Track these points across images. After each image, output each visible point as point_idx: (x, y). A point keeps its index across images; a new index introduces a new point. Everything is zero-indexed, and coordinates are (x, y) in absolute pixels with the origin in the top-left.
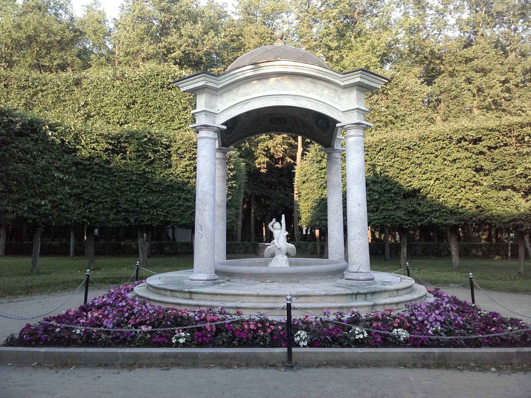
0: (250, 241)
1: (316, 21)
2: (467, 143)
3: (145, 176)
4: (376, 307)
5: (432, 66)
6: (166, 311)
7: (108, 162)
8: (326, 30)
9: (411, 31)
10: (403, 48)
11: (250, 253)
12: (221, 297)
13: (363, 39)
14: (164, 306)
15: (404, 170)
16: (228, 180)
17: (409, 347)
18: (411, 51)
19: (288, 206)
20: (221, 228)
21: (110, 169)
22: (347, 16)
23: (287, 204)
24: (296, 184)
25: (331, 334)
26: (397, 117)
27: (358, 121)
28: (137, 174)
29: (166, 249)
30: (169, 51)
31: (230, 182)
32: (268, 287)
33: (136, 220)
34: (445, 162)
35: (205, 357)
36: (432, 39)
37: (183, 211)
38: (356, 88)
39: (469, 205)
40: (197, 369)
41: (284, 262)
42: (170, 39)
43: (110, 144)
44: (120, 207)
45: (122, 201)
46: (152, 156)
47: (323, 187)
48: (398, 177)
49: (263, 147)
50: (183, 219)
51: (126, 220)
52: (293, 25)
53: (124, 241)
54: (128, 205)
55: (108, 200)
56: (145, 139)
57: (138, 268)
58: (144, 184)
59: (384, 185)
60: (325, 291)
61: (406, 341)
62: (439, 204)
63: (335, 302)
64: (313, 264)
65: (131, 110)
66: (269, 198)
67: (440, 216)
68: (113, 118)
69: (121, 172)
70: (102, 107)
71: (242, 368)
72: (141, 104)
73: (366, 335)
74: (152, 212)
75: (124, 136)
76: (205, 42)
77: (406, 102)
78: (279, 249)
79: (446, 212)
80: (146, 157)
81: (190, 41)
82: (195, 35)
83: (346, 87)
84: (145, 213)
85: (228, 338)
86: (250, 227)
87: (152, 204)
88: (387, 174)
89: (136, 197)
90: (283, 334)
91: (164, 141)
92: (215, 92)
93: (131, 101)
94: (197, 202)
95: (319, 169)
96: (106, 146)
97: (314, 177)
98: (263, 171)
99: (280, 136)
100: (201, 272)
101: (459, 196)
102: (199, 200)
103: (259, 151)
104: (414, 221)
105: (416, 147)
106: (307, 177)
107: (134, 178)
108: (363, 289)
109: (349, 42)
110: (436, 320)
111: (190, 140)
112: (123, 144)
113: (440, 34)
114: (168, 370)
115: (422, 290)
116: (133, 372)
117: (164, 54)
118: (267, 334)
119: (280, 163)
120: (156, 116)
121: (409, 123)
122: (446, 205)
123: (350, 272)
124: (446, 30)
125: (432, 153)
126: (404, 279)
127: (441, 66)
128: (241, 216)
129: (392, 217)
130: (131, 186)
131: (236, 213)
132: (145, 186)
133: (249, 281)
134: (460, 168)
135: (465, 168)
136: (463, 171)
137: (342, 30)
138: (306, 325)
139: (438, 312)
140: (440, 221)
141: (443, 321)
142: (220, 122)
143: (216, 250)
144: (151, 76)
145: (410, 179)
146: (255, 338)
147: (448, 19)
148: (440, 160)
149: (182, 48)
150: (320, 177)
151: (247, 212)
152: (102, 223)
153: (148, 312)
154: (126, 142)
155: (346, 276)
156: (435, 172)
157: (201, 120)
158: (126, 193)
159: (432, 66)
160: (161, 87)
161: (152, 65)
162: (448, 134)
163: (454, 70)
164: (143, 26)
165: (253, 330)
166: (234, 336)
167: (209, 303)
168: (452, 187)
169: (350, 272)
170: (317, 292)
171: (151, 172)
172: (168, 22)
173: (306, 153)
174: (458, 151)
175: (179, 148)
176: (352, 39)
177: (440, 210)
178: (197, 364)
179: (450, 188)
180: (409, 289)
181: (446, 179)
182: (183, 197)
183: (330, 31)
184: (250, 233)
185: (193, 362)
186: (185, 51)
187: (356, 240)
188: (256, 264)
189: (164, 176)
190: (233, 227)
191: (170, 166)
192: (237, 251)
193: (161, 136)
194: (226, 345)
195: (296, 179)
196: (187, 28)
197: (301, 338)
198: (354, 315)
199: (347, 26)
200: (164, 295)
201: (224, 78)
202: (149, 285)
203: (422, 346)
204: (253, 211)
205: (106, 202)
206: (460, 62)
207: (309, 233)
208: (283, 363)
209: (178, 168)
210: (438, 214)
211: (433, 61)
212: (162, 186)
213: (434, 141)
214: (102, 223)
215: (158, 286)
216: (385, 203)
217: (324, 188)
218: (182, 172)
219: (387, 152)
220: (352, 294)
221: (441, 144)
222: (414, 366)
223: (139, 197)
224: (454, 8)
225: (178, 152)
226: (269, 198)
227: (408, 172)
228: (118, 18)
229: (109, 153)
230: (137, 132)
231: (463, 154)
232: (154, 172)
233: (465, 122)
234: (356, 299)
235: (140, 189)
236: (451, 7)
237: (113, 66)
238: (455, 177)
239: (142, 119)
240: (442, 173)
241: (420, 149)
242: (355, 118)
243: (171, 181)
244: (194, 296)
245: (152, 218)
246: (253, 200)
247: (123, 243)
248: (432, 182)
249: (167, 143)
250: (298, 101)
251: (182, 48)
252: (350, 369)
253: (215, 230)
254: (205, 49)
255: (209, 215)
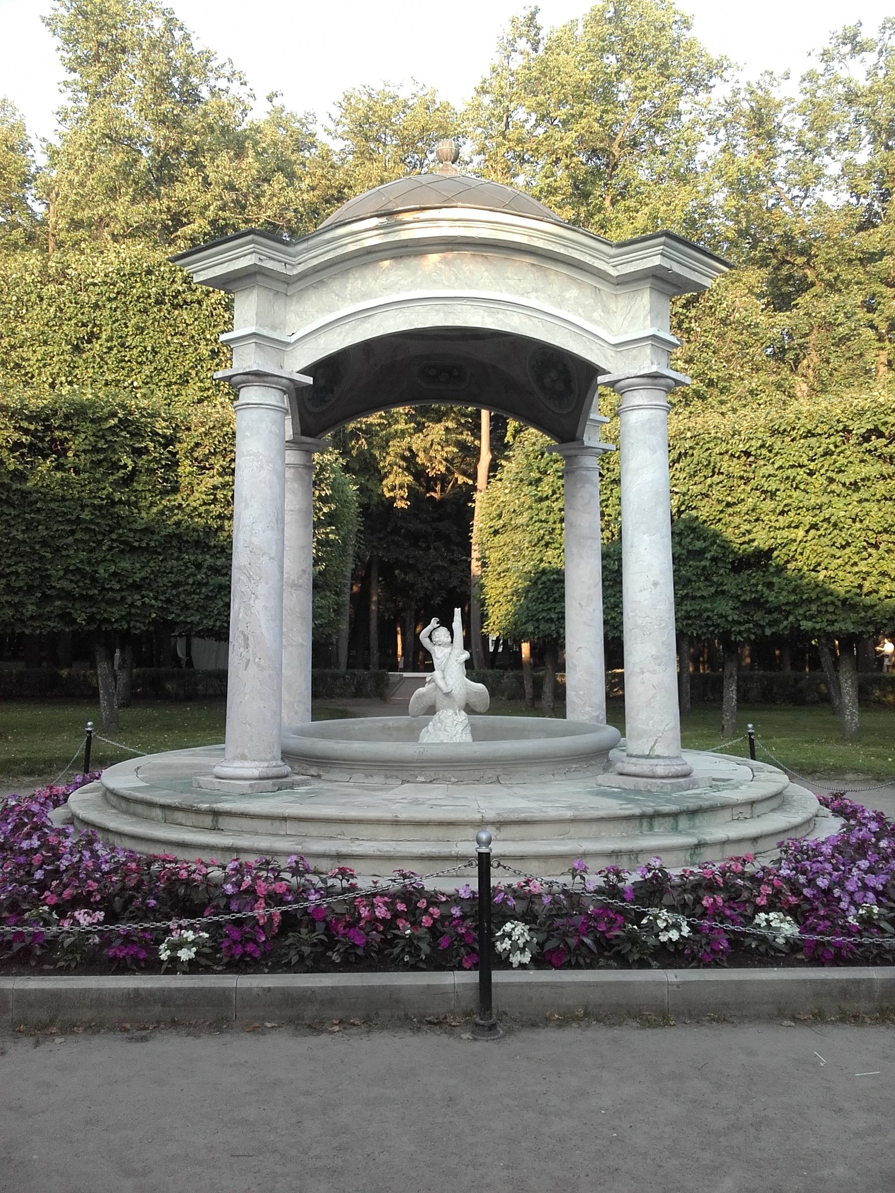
0: (368, 668)
1: (523, 161)
2: (884, 441)
3: (112, 510)
4: (703, 850)
5: (784, 272)
6: (149, 865)
7: (21, 476)
8: (548, 181)
9: (745, 186)
10: (725, 226)
11: (368, 696)
12: (296, 825)
13: (631, 203)
14: (142, 849)
15: (734, 504)
16: (317, 525)
17: (801, 963)
18: (742, 233)
19: (455, 587)
20: (299, 639)
21: (25, 494)
22: (594, 151)
23: (455, 582)
24: (475, 537)
25: (595, 929)
26: (711, 383)
27: (654, 369)
28: (94, 506)
29: (168, 686)
30: (178, 220)
31: (322, 530)
32: (420, 796)
33: (91, 619)
34: (833, 487)
35: (250, 999)
36: (786, 209)
37: (207, 598)
38: (647, 284)
39: (887, 587)
40: (227, 1038)
41: (460, 728)
42: (179, 191)
43: (26, 432)
44: (52, 587)
45: (55, 571)
46: (130, 463)
47: (543, 542)
48: (720, 520)
49: (399, 450)
50: (206, 617)
51: (66, 617)
52: (470, 167)
53: (69, 666)
54: (72, 581)
55: (21, 569)
56: (113, 422)
57: (89, 739)
58: (111, 532)
59: (688, 540)
60: (569, 807)
61: (793, 945)
62: (817, 586)
63: (597, 838)
64: (529, 734)
65: (84, 356)
66: (413, 567)
67: (820, 612)
68: (39, 374)
69: (53, 500)
70: (13, 347)
71: (354, 1030)
72: (107, 341)
73: (686, 931)
74: (129, 600)
75: (60, 414)
76: (263, 201)
77: (730, 348)
78: (448, 695)
79: (833, 603)
80: (116, 466)
81: (228, 196)
82: (242, 183)
83: (624, 282)
84: (112, 602)
85: (314, 945)
86: (368, 632)
87: (131, 581)
88: (694, 513)
89: (89, 562)
90: (466, 932)
91: (160, 426)
92: (285, 286)
93: (83, 332)
94: (235, 574)
95: (536, 501)
96: (16, 436)
97: (522, 520)
98: (400, 504)
99: (438, 425)
100: (243, 757)
101: (863, 567)
102: (240, 568)
103: (389, 459)
104: (757, 624)
105: (764, 451)
106: (505, 518)
107: (86, 515)
108: (668, 801)
109: (600, 209)
110: (865, 887)
111: (223, 425)
112: (57, 433)
113: (806, 197)
114: (144, 1039)
115: (806, 798)
116: (44, 1048)
117: (165, 227)
118: (421, 932)
119: (438, 488)
120: (147, 370)
121: (739, 398)
122: (832, 586)
123: (629, 756)
124: (820, 187)
125: (801, 466)
126: (760, 770)
127: (808, 272)
128: (347, 611)
129: (705, 615)
130: (78, 536)
131: (337, 604)
132: (114, 536)
133: (370, 780)
134: (867, 500)
135: (879, 501)
136: (872, 507)
137: (584, 182)
138: (526, 906)
139: (867, 863)
140: (818, 626)
141: (881, 888)
142: (295, 364)
143: (285, 696)
144: (133, 275)
145: (748, 527)
146: (389, 943)
147: (825, 162)
148: (819, 481)
149: (210, 213)
150: (536, 518)
151: (360, 601)
152: (6, 626)
153: (98, 869)
154: (65, 429)
155: (619, 766)
156: (808, 510)
157: (246, 360)
158: (64, 553)
159: (784, 272)
160: (158, 302)
161: (134, 250)
162: (838, 421)
163: (836, 278)
164: (118, 159)
165: (383, 921)
166: (330, 937)
167: (263, 843)
168: (848, 544)
169: (629, 756)
170: (552, 813)
171: (128, 503)
172: (177, 151)
173: (503, 463)
174: (862, 461)
175: (197, 445)
176: (607, 203)
177: (818, 598)
178: (227, 1020)
179: (843, 547)
180: (778, 801)
181: (835, 525)
182: (206, 565)
183: (557, 184)
184: (368, 648)
185: (216, 1017)
186: (217, 221)
187: (647, 675)
188: (387, 734)
189: (161, 513)
190: (329, 636)
191: (175, 490)
192: (337, 691)
193: (151, 416)
194: (309, 963)
195: (478, 523)
196: (221, 166)
197: (514, 944)
198: (649, 875)
199: (596, 173)
200: (147, 818)
201: (308, 250)
202: (108, 789)
203: (839, 960)
204: (375, 598)
205: (16, 573)
206: (850, 261)
207: (500, 650)
208: (468, 1014)
209: (196, 494)
210: (814, 607)
211: (788, 258)
212: (156, 537)
213: (806, 437)
214: (6, 626)
215: (134, 795)
216: (690, 581)
217: (547, 545)
218: (205, 504)
219: (695, 462)
220: (642, 817)
221: (826, 443)
222: (819, 1017)
223: (98, 563)
224: (838, 139)
225: (196, 455)
226: (413, 567)
227: (745, 509)
228: (57, 143)
229: (22, 455)
230: (92, 404)
231: (873, 469)
232: (136, 502)
233: (858, 398)
234: (651, 828)
235: (100, 543)
236: (832, 136)
237: (44, 250)
238: (854, 521)
239: (110, 377)
240: (826, 513)
241: (772, 455)
242: (647, 362)
243: (178, 524)
244: (223, 822)
245: (129, 613)
246: (374, 573)
247: (64, 673)
248: (801, 533)
249: (169, 432)
250: (500, 316)
251: (210, 213)
252: (649, 1032)
253: (281, 647)
254: (263, 217)
255: (265, 608)
